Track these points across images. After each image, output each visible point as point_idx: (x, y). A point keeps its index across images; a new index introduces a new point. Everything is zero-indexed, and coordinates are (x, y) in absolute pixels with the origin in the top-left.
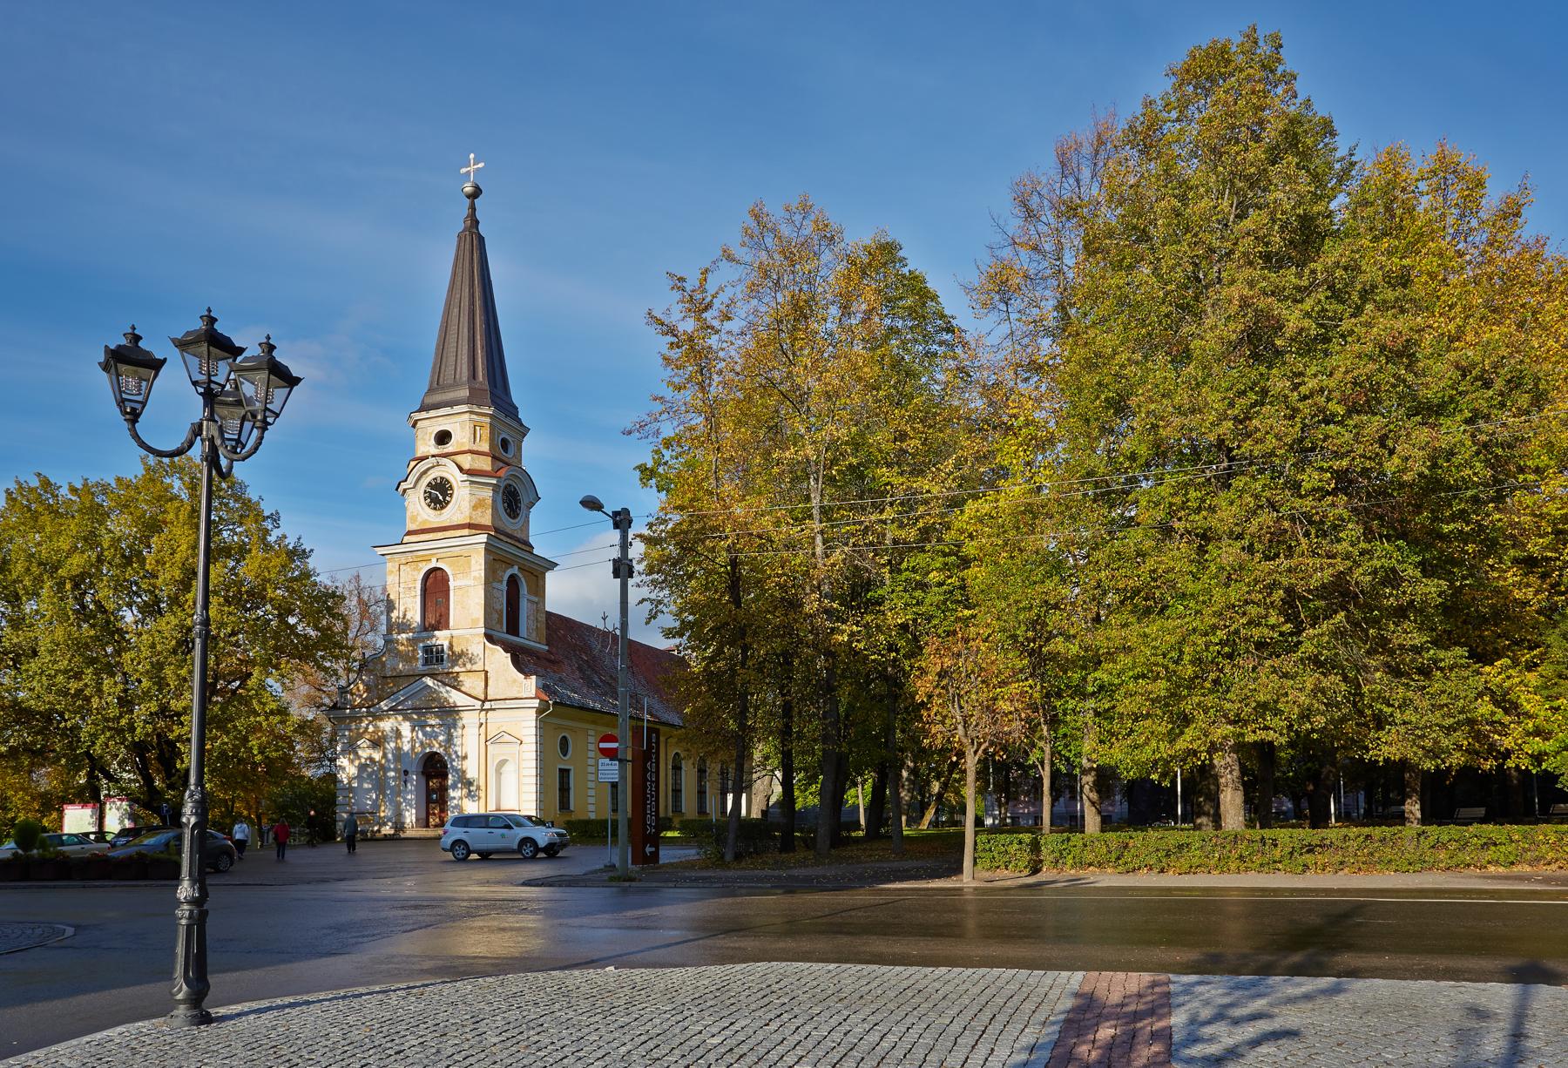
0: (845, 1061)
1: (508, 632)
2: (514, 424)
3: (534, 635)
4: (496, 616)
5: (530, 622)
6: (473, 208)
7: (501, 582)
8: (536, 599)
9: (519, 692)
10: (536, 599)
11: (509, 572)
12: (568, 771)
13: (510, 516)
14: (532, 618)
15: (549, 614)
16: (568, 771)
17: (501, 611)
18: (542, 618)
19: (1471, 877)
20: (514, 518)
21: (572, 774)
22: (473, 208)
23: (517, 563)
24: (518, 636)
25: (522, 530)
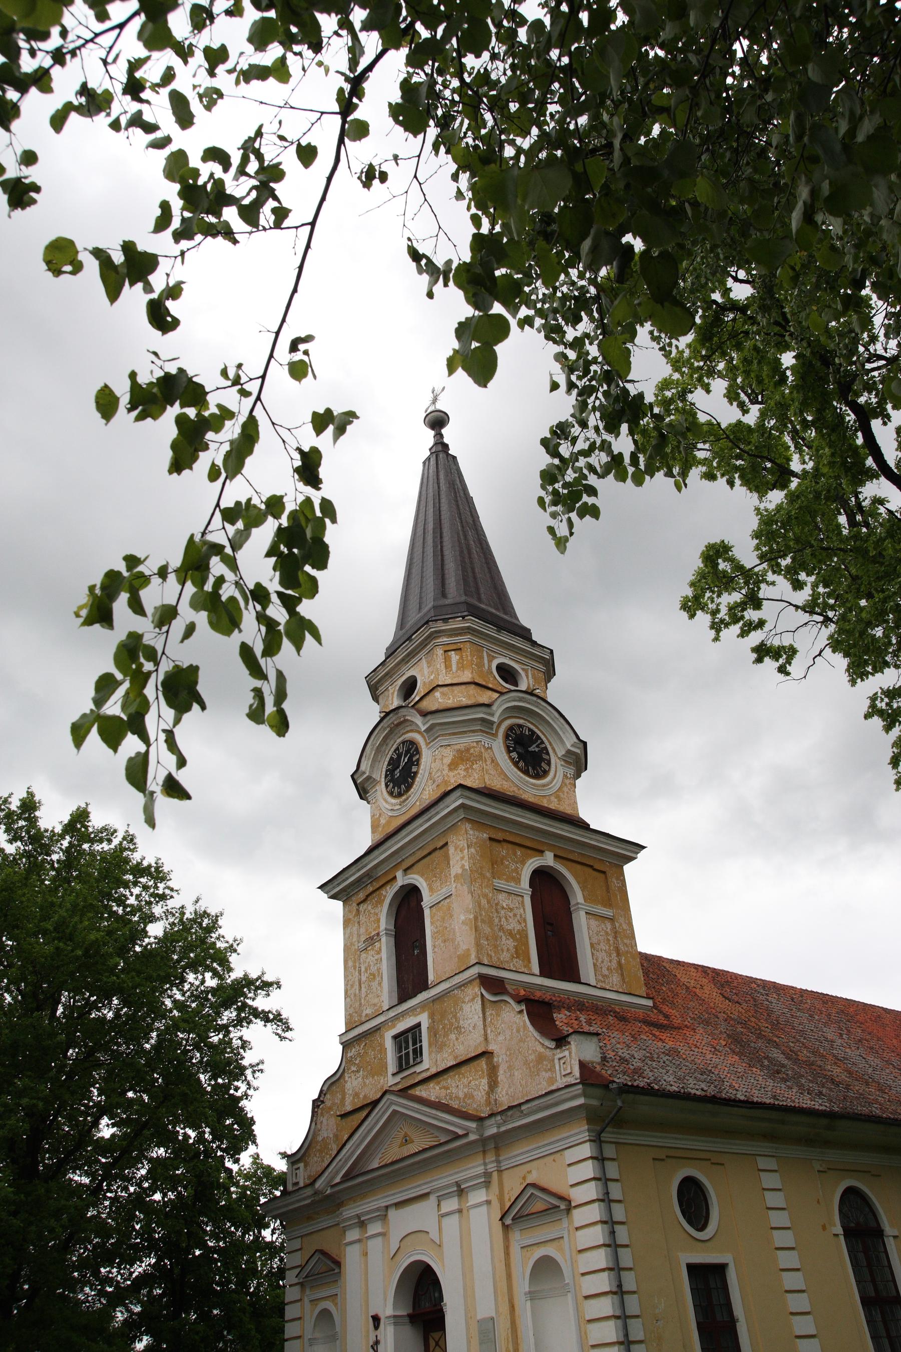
0: (355, 1022)
1: (545, 972)
2: (526, 647)
3: (615, 979)
4: (511, 943)
5: (601, 955)
6: (439, 436)
7: (518, 880)
8: (608, 912)
9: (552, 1080)
10: (608, 912)
11: (533, 863)
12: (721, 1269)
13: (526, 772)
14: (603, 946)
15: (646, 958)
16: (721, 1269)
17: (523, 934)
18: (635, 965)
19: (385, 1335)
20: (537, 776)
21: (732, 1276)
22: (439, 436)
23: (551, 848)
24: (576, 979)
25: (558, 797)
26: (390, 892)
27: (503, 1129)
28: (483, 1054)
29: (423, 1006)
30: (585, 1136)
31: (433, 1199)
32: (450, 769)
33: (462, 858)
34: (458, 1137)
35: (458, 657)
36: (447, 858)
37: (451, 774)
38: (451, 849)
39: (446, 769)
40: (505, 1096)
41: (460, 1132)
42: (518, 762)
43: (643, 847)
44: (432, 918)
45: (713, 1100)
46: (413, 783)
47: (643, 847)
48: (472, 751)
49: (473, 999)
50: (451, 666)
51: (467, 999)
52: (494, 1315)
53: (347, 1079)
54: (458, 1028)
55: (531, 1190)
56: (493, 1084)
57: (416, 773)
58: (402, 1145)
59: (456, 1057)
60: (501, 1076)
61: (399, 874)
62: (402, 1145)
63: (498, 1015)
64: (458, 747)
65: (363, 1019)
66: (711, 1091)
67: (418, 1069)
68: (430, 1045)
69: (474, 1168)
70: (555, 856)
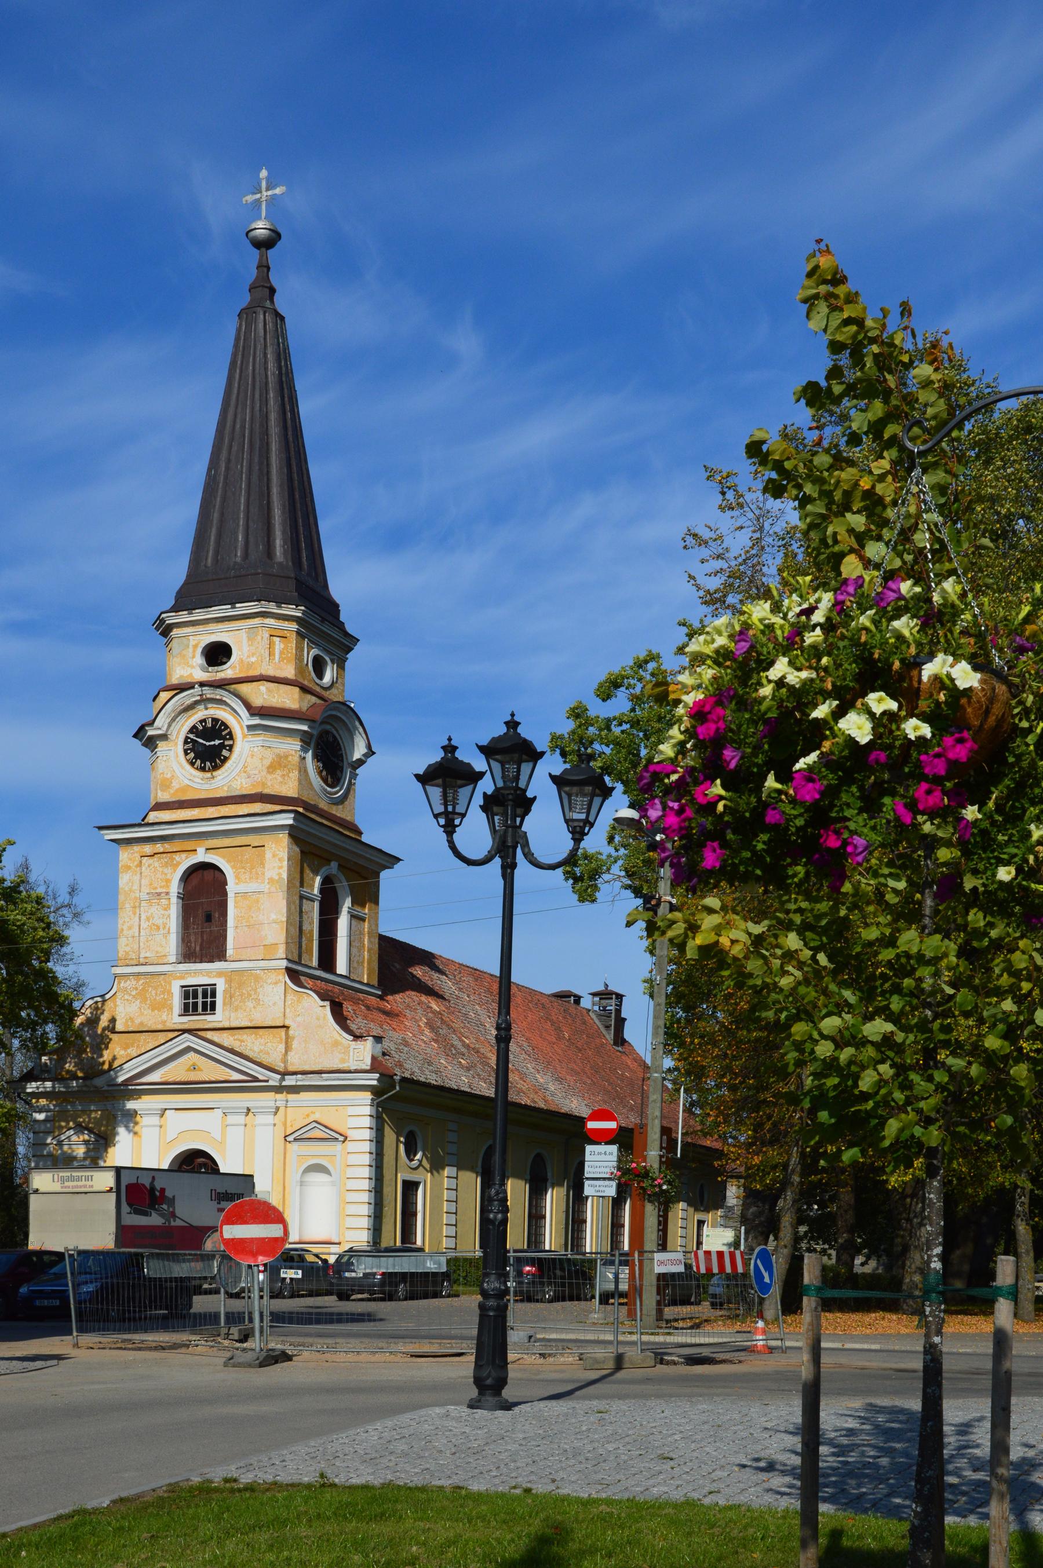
6: (264, 267)
9: (343, 1061)
22: (264, 267)
23: (337, 858)
26: (187, 862)
27: (299, 1083)
28: (283, 1027)
29: (220, 974)
30: (369, 1102)
31: (218, 1113)
32: (269, 772)
33: (281, 867)
34: (257, 1080)
35: (282, 646)
36: (262, 857)
37: (269, 777)
38: (266, 848)
39: (265, 771)
40: (295, 1062)
41: (261, 1077)
42: (321, 771)
43: (398, 860)
44: (236, 902)
45: (441, 1088)
46: (221, 766)
47: (398, 860)
48: (290, 758)
49: (276, 983)
50: (274, 655)
51: (269, 981)
52: (270, 1190)
53: (118, 1002)
54: (258, 1000)
55: (315, 1125)
56: (288, 1049)
57: (226, 759)
58: (189, 1070)
59: (251, 1021)
60: (295, 1044)
61: (201, 850)
62: (189, 1070)
63: (299, 1001)
64: (277, 751)
65: (142, 961)
66: (440, 1083)
67: (209, 1018)
68: (224, 1004)
69: (267, 1099)
70: (339, 865)
